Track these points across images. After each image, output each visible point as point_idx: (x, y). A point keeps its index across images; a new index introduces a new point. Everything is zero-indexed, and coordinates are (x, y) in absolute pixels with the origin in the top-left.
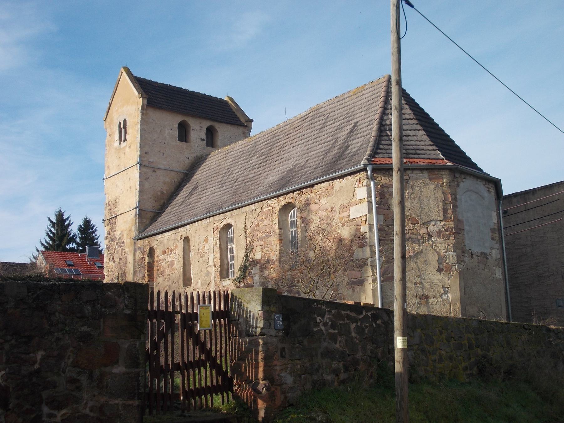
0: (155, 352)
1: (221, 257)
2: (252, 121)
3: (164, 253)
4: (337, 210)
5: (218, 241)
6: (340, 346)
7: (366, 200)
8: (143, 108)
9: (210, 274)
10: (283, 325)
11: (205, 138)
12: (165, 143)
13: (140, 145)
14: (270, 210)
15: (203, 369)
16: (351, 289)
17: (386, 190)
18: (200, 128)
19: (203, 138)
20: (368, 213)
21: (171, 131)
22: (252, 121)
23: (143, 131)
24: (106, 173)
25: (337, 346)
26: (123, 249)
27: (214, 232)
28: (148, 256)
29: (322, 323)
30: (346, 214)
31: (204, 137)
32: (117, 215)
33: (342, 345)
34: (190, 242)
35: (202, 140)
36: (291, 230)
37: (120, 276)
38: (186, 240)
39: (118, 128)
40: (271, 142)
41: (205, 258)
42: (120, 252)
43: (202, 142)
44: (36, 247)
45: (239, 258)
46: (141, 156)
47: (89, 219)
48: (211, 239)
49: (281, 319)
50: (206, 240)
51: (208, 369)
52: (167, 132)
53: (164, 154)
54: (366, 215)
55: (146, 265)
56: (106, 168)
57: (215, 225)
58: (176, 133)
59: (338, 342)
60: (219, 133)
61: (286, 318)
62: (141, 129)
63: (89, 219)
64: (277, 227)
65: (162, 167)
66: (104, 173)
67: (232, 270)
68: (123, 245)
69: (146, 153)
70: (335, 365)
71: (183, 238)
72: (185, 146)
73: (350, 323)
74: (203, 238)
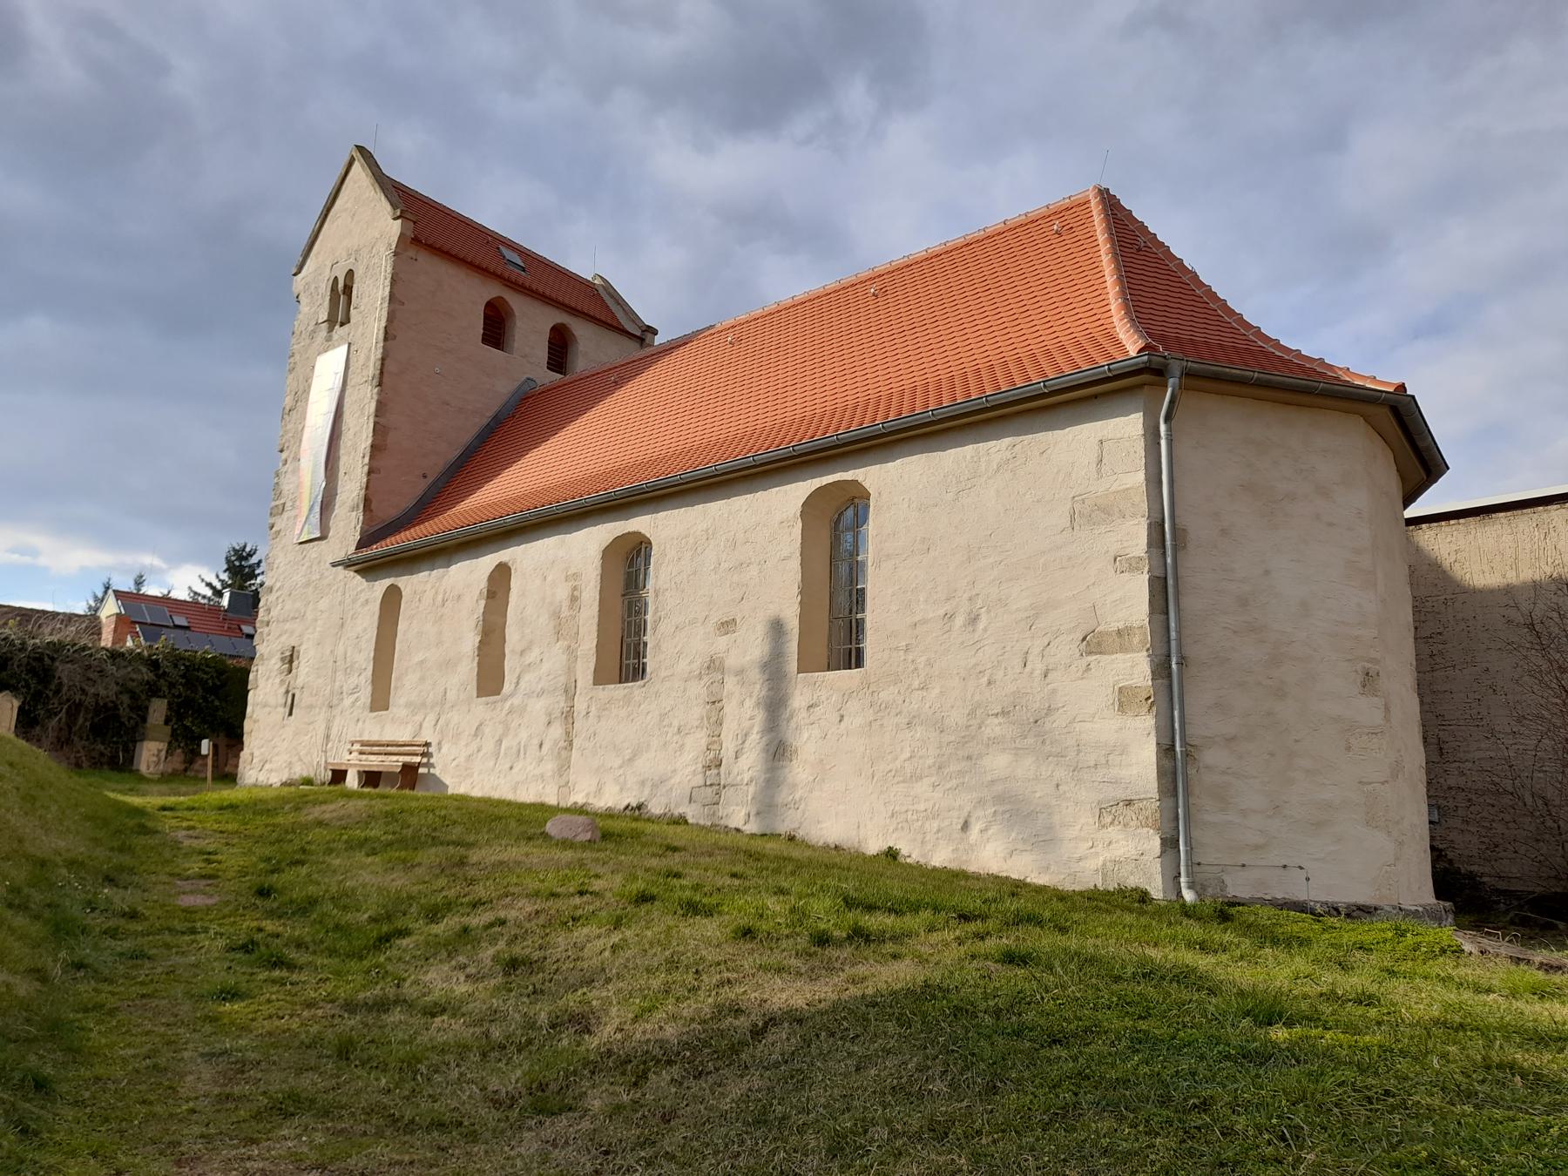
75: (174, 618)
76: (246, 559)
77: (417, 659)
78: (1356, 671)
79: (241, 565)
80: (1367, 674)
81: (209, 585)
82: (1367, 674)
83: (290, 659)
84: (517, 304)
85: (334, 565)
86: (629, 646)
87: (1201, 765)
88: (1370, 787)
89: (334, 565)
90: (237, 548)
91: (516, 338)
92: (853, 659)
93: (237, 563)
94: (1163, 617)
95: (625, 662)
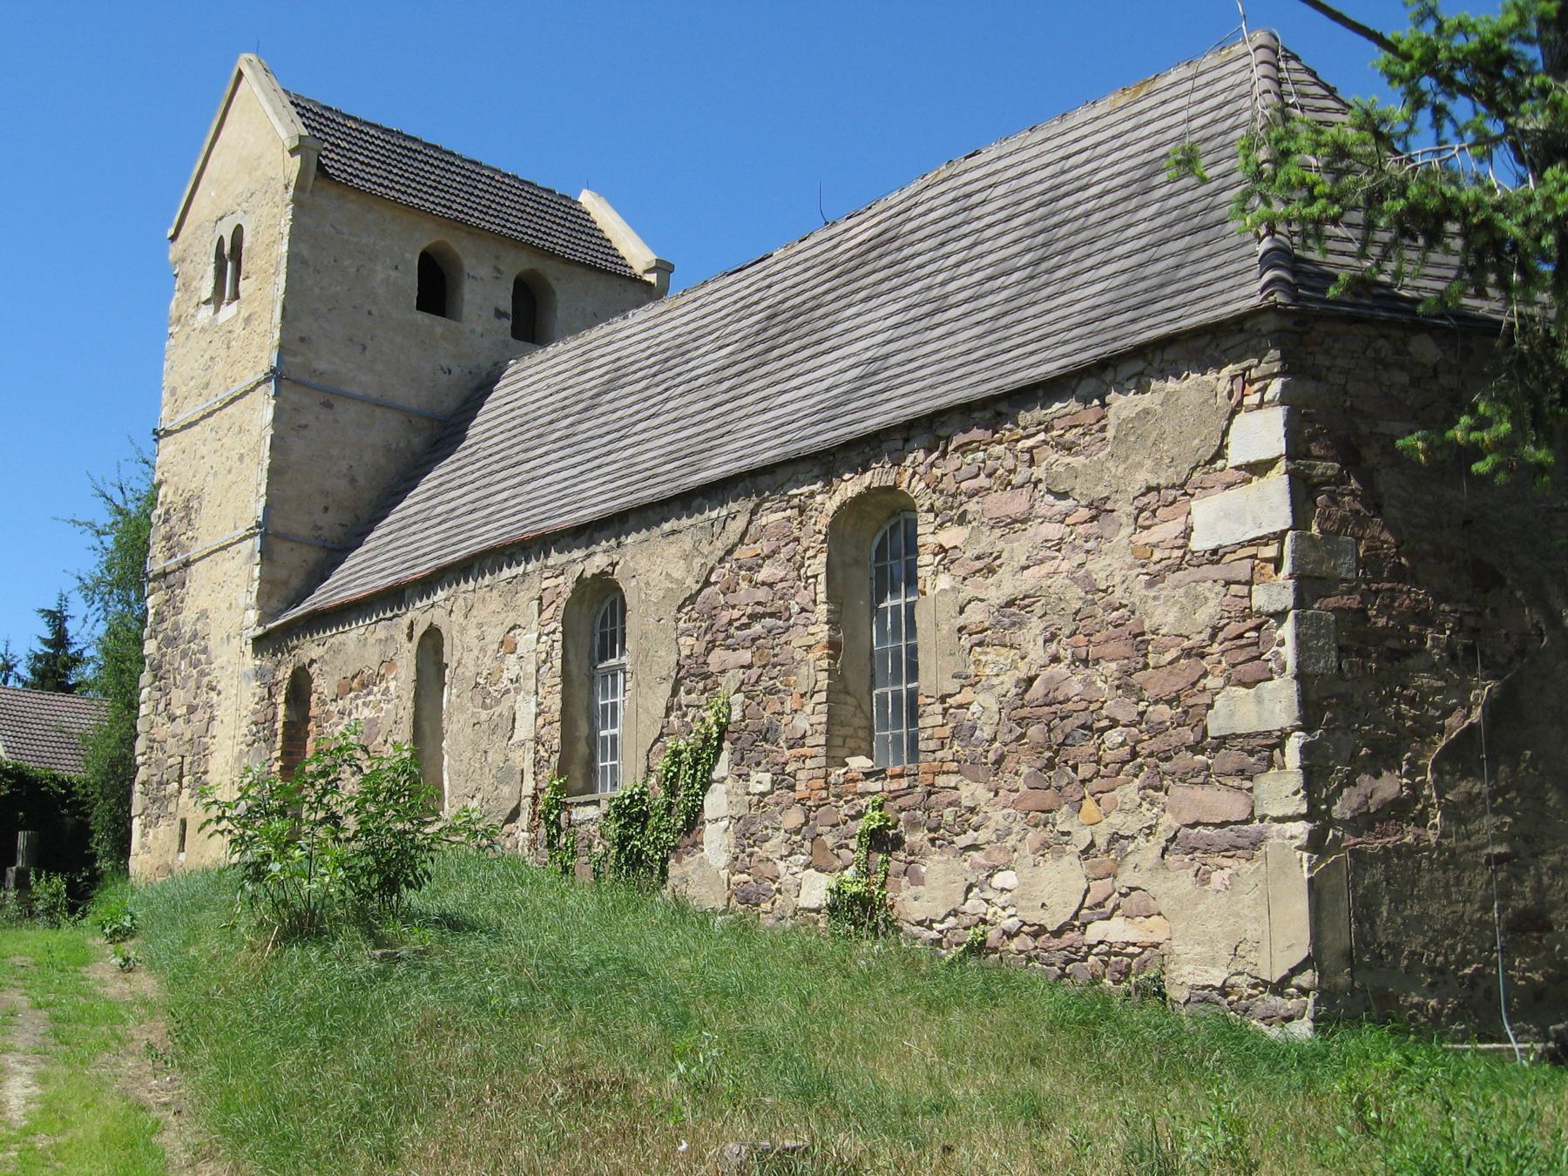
1: (563, 711)
3: (344, 690)
4: (1124, 509)
5: (558, 645)
7: (1282, 465)
8: (299, 187)
9: (518, 777)
11: (510, 311)
12: (370, 313)
13: (284, 308)
14: (789, 519)
16: (1191, 872)
17: (1364, 429)
18: (495, 274)
19: (501, 309)
20: (1289, 522)
21: (393, 274)
23: (296, 262)
24: (165, 413)
26: (203, 674)
27: (540, 612)
28: (287, 701)
30: (1166, 531)
31: (506, 304)
32: (193, 555)
34: (446, 649)
35: (499, 314)
36: (601, 703)
37: (186, 768)
38: (429, 642)
39: (213, 260)
40: (740, 330)
41: (503, 708)
42: (192, 684)
43: (497, 322)
45: (643, 716)
46: (283, 349)
48: (526, 640)
50: (507, 645)
52: (380, 276)
53: (364, 348)
54: (1284, 533)
55: (280, 731)
56: (165, 395)
57: (545, 584)
58: (411, 282)
60: (558, 293)
62: (292, 257)
64: (821, 588)
65: (354, 390)
66: (158, 407)
67: (609, 763)
68: (203, 657)
69: (302, 340)
71: (419, 631)
72: (439, 330)
74: (495, 634)
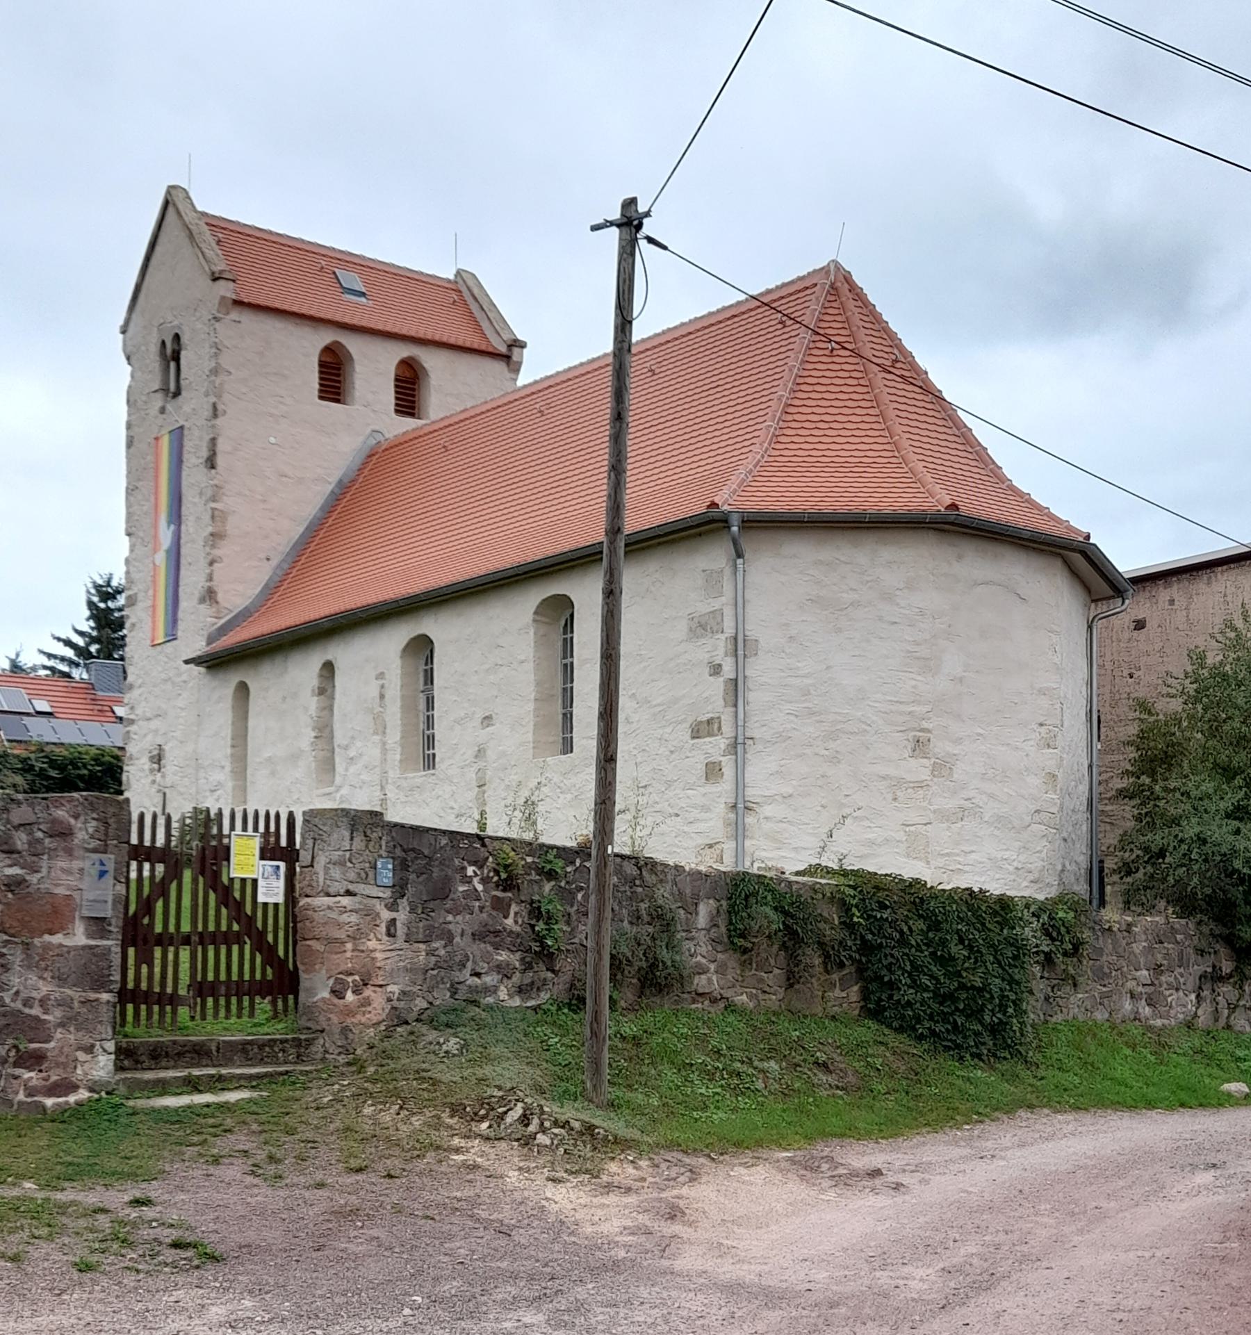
0: (146, 921)
2: (522, 345)
6: (516, 922)
10: (394, 877)
15: (235, 948)
22: (522, 345)
25: (509, 922)
29: (478, 878)
33: (520, 922)
44: (59, 639)
47: (88, 619)
49: (390, 866)
51: (247, 948)
59: (512, 915)
61: (402, 866)
63: (88, 619)
70: (503, 956)
73: (541, 880)
75: (33, 701)
76: (112, 596)
77: (267, 755)
78: (908, 740)
79: (108, 608)
80: (918, 741)
81: (68, 643)
82: (918, 741)
83: (158, 759)
84: (354, 345)
85: (187, 662)
86: (428, 737)
87: (762, 816)
88: (912, 828)
89: (187, 662)
90: (100, 582)
91: (357, 386)
92: (430, 762)
93: (102, 605)
94: (733, 709)
95: (427, 752)
